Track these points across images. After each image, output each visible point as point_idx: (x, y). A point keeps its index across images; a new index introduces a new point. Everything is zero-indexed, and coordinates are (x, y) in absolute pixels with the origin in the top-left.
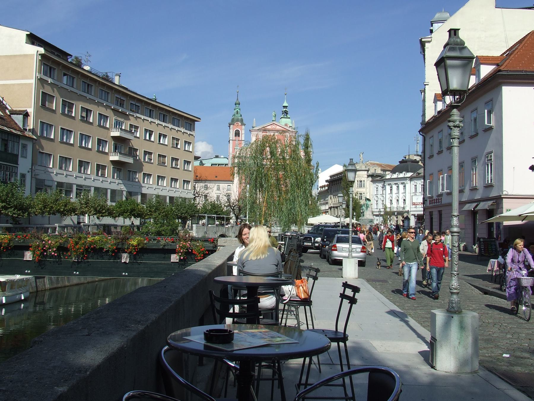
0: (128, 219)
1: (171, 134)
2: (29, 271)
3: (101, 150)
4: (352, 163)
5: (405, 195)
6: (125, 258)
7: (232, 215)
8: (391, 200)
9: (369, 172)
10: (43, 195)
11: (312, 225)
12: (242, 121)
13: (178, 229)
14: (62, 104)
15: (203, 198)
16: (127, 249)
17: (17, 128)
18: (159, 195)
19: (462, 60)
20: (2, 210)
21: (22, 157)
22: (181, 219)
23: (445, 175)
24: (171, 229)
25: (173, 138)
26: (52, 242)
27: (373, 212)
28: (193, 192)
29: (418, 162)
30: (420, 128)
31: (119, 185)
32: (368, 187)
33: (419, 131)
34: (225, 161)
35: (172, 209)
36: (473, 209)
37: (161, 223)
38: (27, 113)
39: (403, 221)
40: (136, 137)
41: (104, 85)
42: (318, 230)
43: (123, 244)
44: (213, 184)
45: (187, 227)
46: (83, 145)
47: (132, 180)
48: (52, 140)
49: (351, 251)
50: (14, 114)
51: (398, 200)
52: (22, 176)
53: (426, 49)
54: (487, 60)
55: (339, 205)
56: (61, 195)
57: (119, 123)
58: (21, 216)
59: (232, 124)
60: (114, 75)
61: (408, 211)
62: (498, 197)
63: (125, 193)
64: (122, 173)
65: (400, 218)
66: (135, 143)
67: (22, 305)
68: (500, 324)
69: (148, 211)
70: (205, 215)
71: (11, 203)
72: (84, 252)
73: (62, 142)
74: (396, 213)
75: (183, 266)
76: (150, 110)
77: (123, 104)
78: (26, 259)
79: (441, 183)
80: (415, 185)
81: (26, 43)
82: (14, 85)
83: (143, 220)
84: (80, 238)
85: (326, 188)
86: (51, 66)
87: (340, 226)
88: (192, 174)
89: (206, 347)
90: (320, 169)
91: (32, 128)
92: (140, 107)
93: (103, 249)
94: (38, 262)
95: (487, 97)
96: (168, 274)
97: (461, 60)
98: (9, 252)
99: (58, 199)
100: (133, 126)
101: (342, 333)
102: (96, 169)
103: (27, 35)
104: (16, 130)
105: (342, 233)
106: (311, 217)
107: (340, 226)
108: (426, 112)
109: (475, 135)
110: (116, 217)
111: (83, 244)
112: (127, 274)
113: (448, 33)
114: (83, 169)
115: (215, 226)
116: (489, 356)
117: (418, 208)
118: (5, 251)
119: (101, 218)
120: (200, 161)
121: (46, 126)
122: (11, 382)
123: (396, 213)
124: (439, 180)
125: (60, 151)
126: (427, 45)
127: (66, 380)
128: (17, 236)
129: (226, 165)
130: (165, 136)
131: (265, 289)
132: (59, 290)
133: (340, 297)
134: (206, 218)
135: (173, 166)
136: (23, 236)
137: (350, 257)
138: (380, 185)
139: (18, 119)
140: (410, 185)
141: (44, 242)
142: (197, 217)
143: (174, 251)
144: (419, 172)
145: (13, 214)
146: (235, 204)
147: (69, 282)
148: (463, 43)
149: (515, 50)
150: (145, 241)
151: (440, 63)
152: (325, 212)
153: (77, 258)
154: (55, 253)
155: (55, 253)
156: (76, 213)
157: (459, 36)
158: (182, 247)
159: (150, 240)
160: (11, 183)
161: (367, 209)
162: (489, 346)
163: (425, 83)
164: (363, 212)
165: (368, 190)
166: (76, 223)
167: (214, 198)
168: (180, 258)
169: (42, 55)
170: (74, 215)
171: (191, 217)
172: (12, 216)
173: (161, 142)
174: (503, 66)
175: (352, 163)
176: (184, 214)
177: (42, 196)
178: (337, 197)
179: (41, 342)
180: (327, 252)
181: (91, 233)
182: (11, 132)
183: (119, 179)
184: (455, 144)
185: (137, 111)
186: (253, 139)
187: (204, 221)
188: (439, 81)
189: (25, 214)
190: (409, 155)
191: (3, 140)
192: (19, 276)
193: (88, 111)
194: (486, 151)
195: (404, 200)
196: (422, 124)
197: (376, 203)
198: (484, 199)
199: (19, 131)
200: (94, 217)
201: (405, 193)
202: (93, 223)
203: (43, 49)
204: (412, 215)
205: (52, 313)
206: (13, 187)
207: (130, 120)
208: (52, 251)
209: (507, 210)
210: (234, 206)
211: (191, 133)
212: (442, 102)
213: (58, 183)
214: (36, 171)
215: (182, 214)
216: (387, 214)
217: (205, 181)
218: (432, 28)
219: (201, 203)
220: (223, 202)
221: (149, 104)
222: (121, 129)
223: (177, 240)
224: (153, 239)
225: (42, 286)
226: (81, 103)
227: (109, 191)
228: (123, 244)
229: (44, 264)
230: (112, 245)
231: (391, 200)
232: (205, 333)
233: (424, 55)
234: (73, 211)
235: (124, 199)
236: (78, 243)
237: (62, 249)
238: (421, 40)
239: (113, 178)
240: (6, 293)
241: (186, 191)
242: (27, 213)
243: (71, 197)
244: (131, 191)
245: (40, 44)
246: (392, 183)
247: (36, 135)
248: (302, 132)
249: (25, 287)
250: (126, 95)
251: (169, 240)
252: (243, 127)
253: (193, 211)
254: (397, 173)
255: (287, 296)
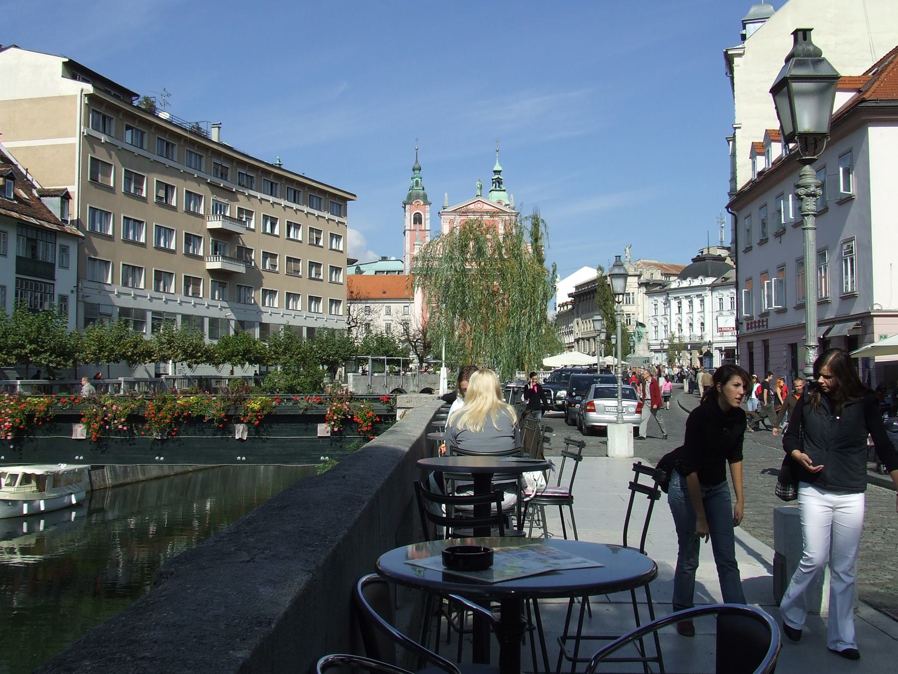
0: (239, 366)
1: (308, 223)
2: (81, 458)
3: (191, 252)
4: (618, 263)
5: (703, 315)
6: (241, 432)
7: (412, 356)
8: (680, 325)
9: (642, 278)
10: (97, 330)
11: (549, 368)
12: (425, 197)
13: (322, 381)
14: (125, 177)
15: (364, 329)
16: (244, 416)
17: (52, 219)
18: (289, 326)
19: (817, 82)
20: (31, 357)
21: (61, 267)
22: (328, 365)
23: (773, 279)
24: (311, 382)
25: (311, 229)
26: (118, 408)
27: (649, 345)
28: (346, 320)
29: (724, 259)
30: (728, 202)
31: (223, 309)
32: (639, 303)
33: (726, 207)
34: (398, 266)
35: (311, 348)
36: (822, 337)
37: (294, 372)
38: (67, 193)
39: (701, 359)
40: (249, 229)
41: (193, 143)
42: (562, 377)
43: (237, 407)
44: (380, 304)
45: (337, 377)
46: (162, 245)
47: (245, 302)
48: (110, 238)
49: (620, 412)
50: (46, 196)
51: (691, 325)
52: (61, 298)
53: (735, 68)
54: (848, 84)
55: (595, 335)
56: (127, 329)
57: (221, 205)
58: (63, 365)
59: (408, 204)
60: (210, 125)
61: (710, 342)
62: (865, 315)
63: (232, 323)
64: (227, 291)
65: (696, 354)
66: (247, 240)
67: (74, 514)
68: (884, 530)
69: (273, 353)
70: (368, 357)
71: (45, 345)
72: (171, 423)
73: (126, 241)
74: (689, 346)
75: (337, 443)
76: (272, 184)
77: (226, 175)
78: (76, 436)
79: (766, 294)
80: (720, 299)
81: (62, 77)
82: (44, 147)
83: (264, 369)
84: (164, 401)
85: (570, 307)
86: (106, 114)
87: (599, 370)
88: (344, 289)
89: (446, 576)
90: (558, 275)
91: (76, 218)
92: (255, 179)
93: (204, 417)
94: (96, 442)
95: (841, 147)
96: (313, 456)
97: (815, 82)
98: (48, 425)
99: (122, 336)
100: (244, 211)
101: (638, 549)
102: (185, 285)
103: (64, 63)
104: (49, 222)
105: (601, 382)
106: (547, 357)
107: (599, 370)
108: (738, 175)
109: (823, 210)
110: (220, 363)
111: (170, 410)
112: (244, 458)
113: (792, 35)
114: (162, 284)
115: (384, 374)
116: (872, 584)
117: (726, 336)
118: (40, 424)
119: (194, 366)
120: (355, 267)
121: (99, 214)
122: (155, 642)
123: (689, 346)
124: (763, 288)
125: (125, 256)
126: (737, 60)
127: (244, 639)
128: (59, 399)
129: (399, 271)
130: (297, 226)
131: (504, 477)
132: (128, 488)
133: (629, 488)
134: (370, 361)
135: (313, 276)
136: (69, 399)
137: (620, 422)
138: (661, 300)
139: (53, 204)
140: (711, 299)
141: (104, 408)
142: (355, 360)
143: (322, 419)
144: (725, 275)
145: (49, 362)
146: (417, 337)
147: (144, 474)
148: (818, 53)
149: (888, 65)
150: (274, 403)
151: (780, 89)
152: (569, 347)
153: (160, 434)
154: (123, 426)
155: (123, 426)
156: (153, 358)
157: (812, 40)
158: (335, 412)
159: (282, 401)
160: (44, 311)
161: (639, 341)
162: (869, 567)
163: (734, 126)
164: (634, 346)
165: (640, 309)
166: (153, 375)
167: (383, 329)
168: (333, 429)
169: (90, 97)
170: (150, 362)
171: (344, 360)
172: (47, 366)
173: (292, 236)
174: (869, 93)
175: (618, 263)
176: (333, 355)
177: (96, 331)
178: (591, 320)
179: (171, 574)
180: (579, 414)
181: (179, 391)
182: (41, 226)
183: (223, 300)
184: (809, 226)
185: (249, 185)
186: (446, 230)
187: (367, 368)
188: (779, 118)
189: (68, 363)
190: (708, 249)
191: (28, 239)
192: (65, 465)
193: (168, 188)
194: (842, 238)
195: (702, 324)
196: (730, 195)
197: (654, 329)
198: (839, 319)
199: (55, 224)
200: (182, 364)
201: (704, 311)
202: (181, 375)
203: (91, 85)
204: (716, 348)
205: (117, 528)
206: (48, 318)
207: (239, 201)
208: (118, 422)
209: (881, 337)
210: (415, 340)
211: (341, 220)
212: (764, 157)
213: (122, 309)
214: (85, 290)
215: (330, 355)
216: (674, 349)
217: (367, 299)
218: (744, 32)
219: (360, 336)
220: (397, 334)
221: (270, 173)
222: (224, 216)
223: (326, 399)
224: (287, 399)
225: (100, 482)
226: (157, 175)
227: (206, 321)
228: (237, 407)
229: (106, 445)
230: (218, 411)
231: (680, 325)
232: (443, 554)
233: (732, 78)
234: (148, 355)
235: (232, 333)
236: (162, 409)
237: (135, 419)
238: (726, 53)
239: (213, 298)
240: (46, 494)
241: (336, 318)
242: (72, 361)
243: (144, 331)
244: (243, 319)
245: (86, 78)
246: (681, 295)
247: (83, 230)
248: (527, 212)
249: (78, 483)
250: (231, 159)
251: (313, 398)
252: (428, 208)
253: (348, 351)
254: (688, 279)
255: (530, 488)
